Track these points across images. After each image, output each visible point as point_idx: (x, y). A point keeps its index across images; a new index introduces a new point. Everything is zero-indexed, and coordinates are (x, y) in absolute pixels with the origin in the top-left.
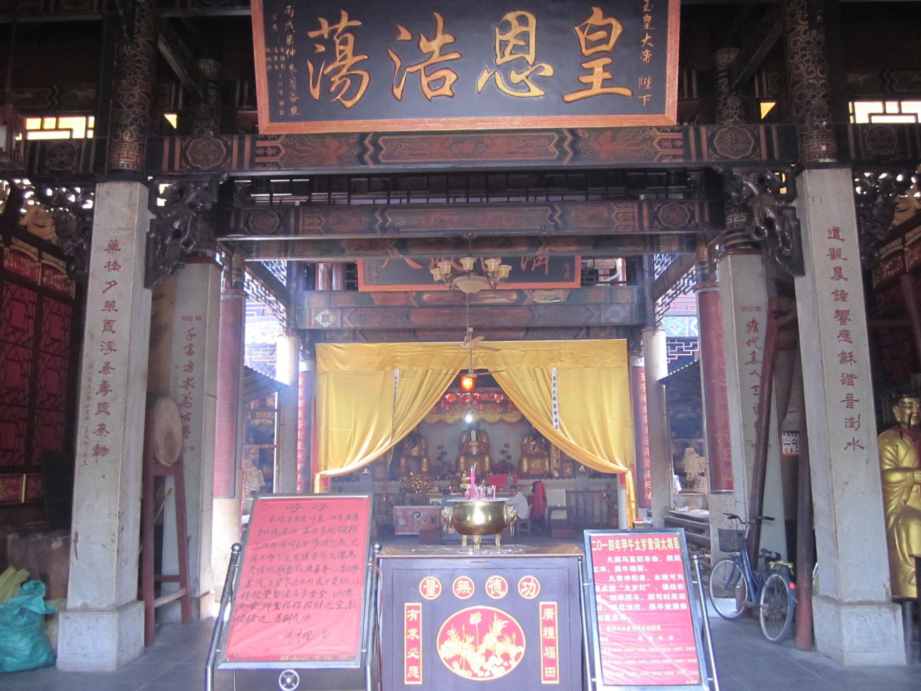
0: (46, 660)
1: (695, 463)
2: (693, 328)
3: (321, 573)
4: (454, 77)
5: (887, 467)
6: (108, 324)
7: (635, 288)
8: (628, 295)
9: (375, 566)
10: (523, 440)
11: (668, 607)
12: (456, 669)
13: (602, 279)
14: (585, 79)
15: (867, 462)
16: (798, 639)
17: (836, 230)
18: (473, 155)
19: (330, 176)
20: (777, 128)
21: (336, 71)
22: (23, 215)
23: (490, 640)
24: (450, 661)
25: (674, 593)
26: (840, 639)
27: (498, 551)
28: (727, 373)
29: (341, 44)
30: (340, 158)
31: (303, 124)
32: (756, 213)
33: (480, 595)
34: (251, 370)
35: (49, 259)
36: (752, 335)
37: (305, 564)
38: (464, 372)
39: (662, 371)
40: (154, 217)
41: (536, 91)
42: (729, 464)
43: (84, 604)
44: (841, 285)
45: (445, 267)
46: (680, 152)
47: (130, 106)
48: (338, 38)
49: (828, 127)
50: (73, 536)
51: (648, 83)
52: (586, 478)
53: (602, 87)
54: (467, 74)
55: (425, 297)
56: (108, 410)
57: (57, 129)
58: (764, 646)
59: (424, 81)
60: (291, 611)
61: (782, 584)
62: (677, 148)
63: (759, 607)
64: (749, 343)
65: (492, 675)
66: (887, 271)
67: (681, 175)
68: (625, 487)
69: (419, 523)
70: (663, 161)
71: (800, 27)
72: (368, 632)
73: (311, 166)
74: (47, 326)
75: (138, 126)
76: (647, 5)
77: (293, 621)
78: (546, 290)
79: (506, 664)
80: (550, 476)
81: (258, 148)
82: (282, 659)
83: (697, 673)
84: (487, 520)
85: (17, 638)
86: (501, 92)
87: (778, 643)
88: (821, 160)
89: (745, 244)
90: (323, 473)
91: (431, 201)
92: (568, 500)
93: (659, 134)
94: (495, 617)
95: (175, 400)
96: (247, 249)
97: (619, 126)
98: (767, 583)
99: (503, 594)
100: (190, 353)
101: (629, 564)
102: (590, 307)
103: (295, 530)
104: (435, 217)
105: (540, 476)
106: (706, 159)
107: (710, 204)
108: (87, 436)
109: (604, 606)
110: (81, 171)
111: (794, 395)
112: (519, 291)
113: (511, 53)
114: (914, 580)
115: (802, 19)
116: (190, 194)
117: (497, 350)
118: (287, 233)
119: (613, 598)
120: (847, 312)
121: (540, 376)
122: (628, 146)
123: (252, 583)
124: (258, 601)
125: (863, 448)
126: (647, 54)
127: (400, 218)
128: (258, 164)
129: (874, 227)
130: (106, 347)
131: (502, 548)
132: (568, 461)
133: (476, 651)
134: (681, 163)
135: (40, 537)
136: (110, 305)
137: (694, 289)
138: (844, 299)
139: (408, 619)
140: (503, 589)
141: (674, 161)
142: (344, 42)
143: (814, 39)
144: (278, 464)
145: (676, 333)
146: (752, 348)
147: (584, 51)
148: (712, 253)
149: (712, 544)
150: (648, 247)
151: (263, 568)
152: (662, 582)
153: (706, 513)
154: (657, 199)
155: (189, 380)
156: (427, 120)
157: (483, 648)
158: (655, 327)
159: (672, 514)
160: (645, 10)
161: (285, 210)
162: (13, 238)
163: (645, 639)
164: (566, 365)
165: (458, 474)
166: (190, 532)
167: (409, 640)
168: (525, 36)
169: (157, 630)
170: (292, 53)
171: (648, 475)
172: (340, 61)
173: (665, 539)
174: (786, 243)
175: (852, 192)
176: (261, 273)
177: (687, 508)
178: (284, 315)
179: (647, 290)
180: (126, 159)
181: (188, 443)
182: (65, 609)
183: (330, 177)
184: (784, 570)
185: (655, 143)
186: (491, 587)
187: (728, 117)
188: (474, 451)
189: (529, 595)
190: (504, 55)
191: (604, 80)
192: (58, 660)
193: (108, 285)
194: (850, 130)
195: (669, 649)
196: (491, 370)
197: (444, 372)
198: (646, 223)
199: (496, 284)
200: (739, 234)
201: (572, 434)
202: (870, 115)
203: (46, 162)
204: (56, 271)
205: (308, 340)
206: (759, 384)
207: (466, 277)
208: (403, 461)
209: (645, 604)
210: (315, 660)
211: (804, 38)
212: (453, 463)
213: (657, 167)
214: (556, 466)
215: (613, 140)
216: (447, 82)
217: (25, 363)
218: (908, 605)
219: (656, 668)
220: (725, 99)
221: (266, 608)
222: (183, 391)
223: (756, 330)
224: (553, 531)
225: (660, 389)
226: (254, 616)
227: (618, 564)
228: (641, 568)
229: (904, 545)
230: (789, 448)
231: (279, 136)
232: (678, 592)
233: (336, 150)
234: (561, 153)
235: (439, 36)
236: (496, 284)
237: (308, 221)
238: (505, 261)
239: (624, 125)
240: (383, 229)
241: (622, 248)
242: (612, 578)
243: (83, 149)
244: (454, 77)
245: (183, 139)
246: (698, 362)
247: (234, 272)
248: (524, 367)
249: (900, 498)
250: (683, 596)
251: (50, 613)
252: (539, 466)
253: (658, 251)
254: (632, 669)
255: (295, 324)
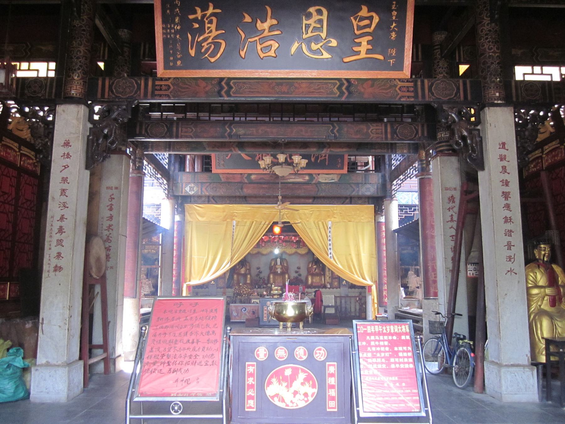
0: (24, 395)
1: (414, 281)
2: (414, 199)
3: (195, 344)
4: (277, 45)
5: (530, 285)
6: (63, 191)
7: (380, 174)
8: (375, 179)
9: (228, 340)
10: (308, 265)
11: (402, 366)
12: (276, 402)
13: (359, 168)
14: (356, 49)
15: (519, 282)
16: (475, 386)
17: (504, 144)
18: (288, 93)
19: (198, 103)
20: (471, 82)
21: (205, 40)
22: (10, 123)
23: (296, 385)
24: (273, 397)
25: (405, 359)
26: (500, 387)
27: (302, 332)
28: (435, 228)
29: (208, 23)
30: (206, 93)
31: (184, 71)
32: (456, 132)
33: (291, 358)
34: (147, 220)
35: (25, 151)
36: (451, 205)
37: (185, 339)
38: (276, 223)
39: (395, 225)
40: (91, 126)
41: (326, 55)
42: (435, 282)
43: (47, 362)
44: (506, 177)
45: (268, 160)
46: (412, 94)
47: (78, 58)
48: (207, 19)
49: (500, 82)
50: (41, 321)
51: (394, 52)
52: (346, 289)
53: (366, 54)
54: (285, 45)
55: (253, 177)
56: (63, 244)
57: (29, 70)
58: (455, 390)
59: (259, 47)
60: (178, 367)
61: (467, 354)
62: (410, 92)
63: (452, 367)
64: (449, 209)
65: (297, 405)
66: (532, 168)
67: (410, 108)
68: (371, 294)
69: (245, 314)
70: (402, 100)
71: (485, 21)
72: (224, 380)
73: (189, 97)
74: (23, 191)
75: (83, 70)
76: (394, 5)
77: (179, 373)
78: (327, 174)
79: (306, 399)
80: (325, 287)
81: (157, 85)
82: (172, 395)
83: (418, 405)
84: (295, 314)
85: (6, 382)
86: (303, 55)
87: (463, 389)
88: (496, 102)
89: (448, 150)
90: (188, 283)
91: (259, 119)
92: (336, 302)
93: (399, 83)
94: (300, 371)
95: (101, 237)
96: (146, 146)
97: (376, 77)
98: (457, 353)
99: (305, 358)
100: (111, 209)
101: (379, 341)
102: (353, 185)
103: (179, 318)
104: (262, 129)
105: (319, 287)
106: (427, 99)
107: (428, 126)
108: (50, 260)
109: (364, 365)
110: (47, 97)
111: (476, 241)
112: (310, 175)
113: (312, 32)
114: (544, 353)
115: (487, 17)
116: (114, 113)
117: (297, 210)
118: (171, 137)
119: (370, 360)
120: (509, 193)
121: (321, 226)
122: (381, 90)
123: (154, 350)
124: (157, 360)
125: (516, 274)
126: (393, 35)
127: (240, 129)
128: (156, 95)
129: (526, 143)
130: (62, 205)
131: (304, 330)
132: (336, 278)
133: (288, 391)
134: (412, 101)
135: (18, 320)
136: (65, 180)
137: (417, 176)
138: (507, 185)
139: (248, 372)
140: (305, 355)
141: (408, 100)
142: (211, 22)
143: (493, 29)
144: (161, 277)
145: (404, 202)
146: (451, 212)
147: (356, 31)
148: (428, 155)
149: (424, 329)
150: (390, 150)
151: (160, 341)
152: (399, 351)
153: (421, 311)
154: (396, 121)
155: (110, 226)
156: (260, 71)
157: (292, 390)
158: (391, 198)
159: (399, 311)
160: (393, 8)
161: (169, 122)
162: (4, 137)
163: (388, 385)
164: (337, 220)
165: (269, 285)
166: (110, 318)
167: (248, 385)
168: (320, 21)
169: (90, 378)
170: (179, 28)
171: (385, 287)
172: (208, 33)
173: (401, 326)
174: (474, 151)
175: (513, 121)
176: (154, 161)
177: (408, 308)
178: (166, 187)
179: (387, 176)
180: (75, 91)
181: (109, 264)
182: (35, 365)
183: (198, 104)
184: (468, 345)
185: (397, 89)
186: (297, 353)
187: (440, 73)
188: (279, 271)
189: (320, 358)
190: (307, 33)
191: (368, 50)
192: (31, 396)
193: (64, 168)
194: (513, 84)
195: (402, 391)
196: (291, 222)
197: (263, 223)
198: (389, 136)
199: (298, 171)
200: (444, 144)
201: (340, 262)
202: (524, 74)
203: (28, 91)
204: (29, 158)
205: (180, 201)
206: (454, 234)
207: (280, 166)
208: (235, 276)
209: (389, 364)
210: (192, 396)
211: (487, 26)
212: (266, 278)
213: (398, 103)
214: (329, 281)
215: (372, 86)
216: (273, 48)
217: (10, 214)
218: (540, 367)
219: (395, 402)
220: (438, 62)
221: (162, 365)
222: (106, 233)
223: (454, 202)
224: (327, 321)
225: (393, 236)
226: (155, 369)
227: (373, 341)
228: (386, 343)
229: (539, 332)
230: (471, 273)
231: (169, 78)
232: (408, 357)
233: (204, 88)
234: (340, 93)
235: (269, 20)
236: (298, 171)
237: (184, 130)
238: (304, 157)
239: (379, 77)
240: (230, 136)
241: (374, 151)
242: (369, 349)
243: (48, 84)
244: (277, 45)
245: (110, 79)
246: (418, 220)
247: (137, 160)
248: (312, 221)
249: (537, 304)
250: (411, 360)
251: (26, 367)
252: (318, 281)
253: (396, 153)
254: (381, 402)
255: (173, 192)
